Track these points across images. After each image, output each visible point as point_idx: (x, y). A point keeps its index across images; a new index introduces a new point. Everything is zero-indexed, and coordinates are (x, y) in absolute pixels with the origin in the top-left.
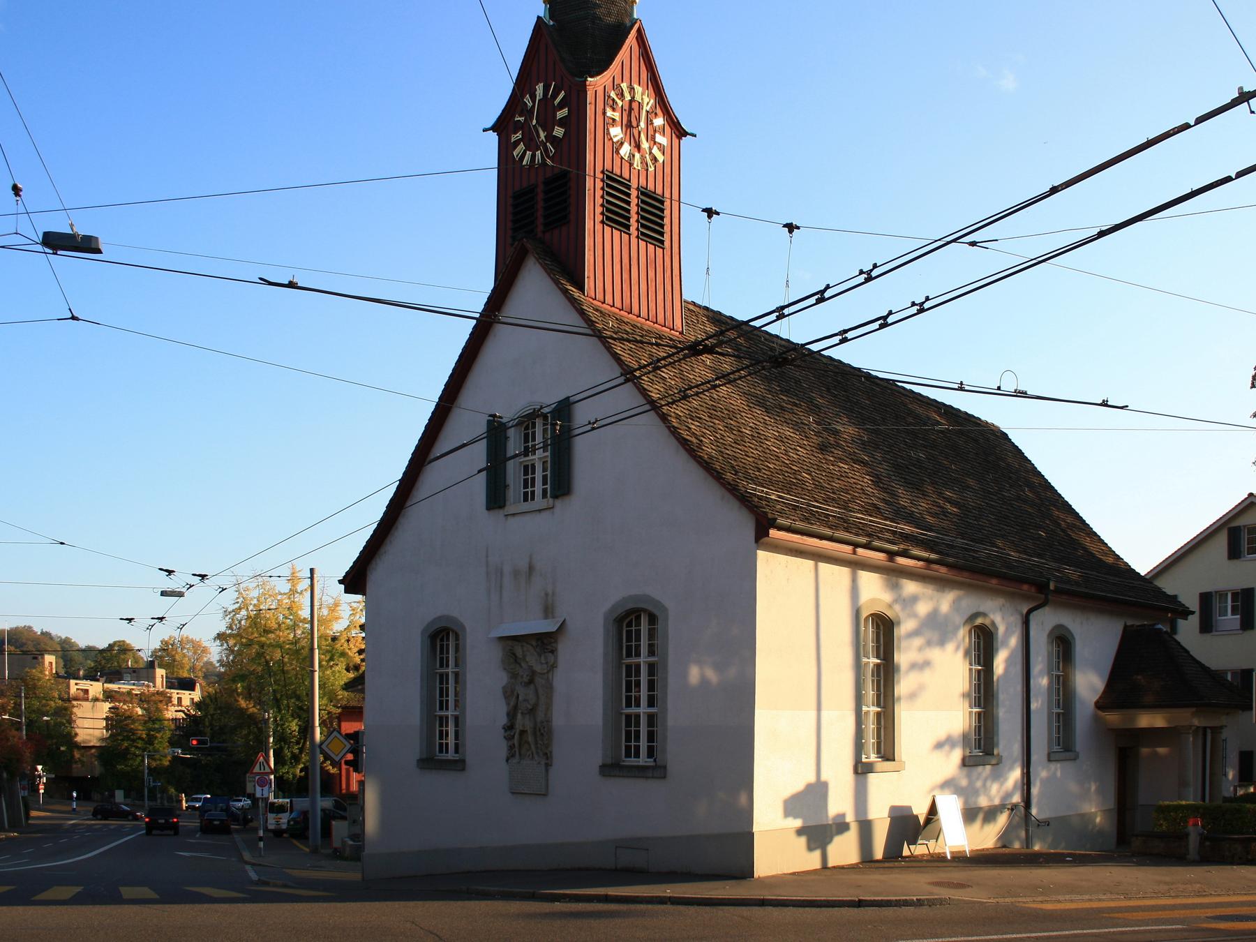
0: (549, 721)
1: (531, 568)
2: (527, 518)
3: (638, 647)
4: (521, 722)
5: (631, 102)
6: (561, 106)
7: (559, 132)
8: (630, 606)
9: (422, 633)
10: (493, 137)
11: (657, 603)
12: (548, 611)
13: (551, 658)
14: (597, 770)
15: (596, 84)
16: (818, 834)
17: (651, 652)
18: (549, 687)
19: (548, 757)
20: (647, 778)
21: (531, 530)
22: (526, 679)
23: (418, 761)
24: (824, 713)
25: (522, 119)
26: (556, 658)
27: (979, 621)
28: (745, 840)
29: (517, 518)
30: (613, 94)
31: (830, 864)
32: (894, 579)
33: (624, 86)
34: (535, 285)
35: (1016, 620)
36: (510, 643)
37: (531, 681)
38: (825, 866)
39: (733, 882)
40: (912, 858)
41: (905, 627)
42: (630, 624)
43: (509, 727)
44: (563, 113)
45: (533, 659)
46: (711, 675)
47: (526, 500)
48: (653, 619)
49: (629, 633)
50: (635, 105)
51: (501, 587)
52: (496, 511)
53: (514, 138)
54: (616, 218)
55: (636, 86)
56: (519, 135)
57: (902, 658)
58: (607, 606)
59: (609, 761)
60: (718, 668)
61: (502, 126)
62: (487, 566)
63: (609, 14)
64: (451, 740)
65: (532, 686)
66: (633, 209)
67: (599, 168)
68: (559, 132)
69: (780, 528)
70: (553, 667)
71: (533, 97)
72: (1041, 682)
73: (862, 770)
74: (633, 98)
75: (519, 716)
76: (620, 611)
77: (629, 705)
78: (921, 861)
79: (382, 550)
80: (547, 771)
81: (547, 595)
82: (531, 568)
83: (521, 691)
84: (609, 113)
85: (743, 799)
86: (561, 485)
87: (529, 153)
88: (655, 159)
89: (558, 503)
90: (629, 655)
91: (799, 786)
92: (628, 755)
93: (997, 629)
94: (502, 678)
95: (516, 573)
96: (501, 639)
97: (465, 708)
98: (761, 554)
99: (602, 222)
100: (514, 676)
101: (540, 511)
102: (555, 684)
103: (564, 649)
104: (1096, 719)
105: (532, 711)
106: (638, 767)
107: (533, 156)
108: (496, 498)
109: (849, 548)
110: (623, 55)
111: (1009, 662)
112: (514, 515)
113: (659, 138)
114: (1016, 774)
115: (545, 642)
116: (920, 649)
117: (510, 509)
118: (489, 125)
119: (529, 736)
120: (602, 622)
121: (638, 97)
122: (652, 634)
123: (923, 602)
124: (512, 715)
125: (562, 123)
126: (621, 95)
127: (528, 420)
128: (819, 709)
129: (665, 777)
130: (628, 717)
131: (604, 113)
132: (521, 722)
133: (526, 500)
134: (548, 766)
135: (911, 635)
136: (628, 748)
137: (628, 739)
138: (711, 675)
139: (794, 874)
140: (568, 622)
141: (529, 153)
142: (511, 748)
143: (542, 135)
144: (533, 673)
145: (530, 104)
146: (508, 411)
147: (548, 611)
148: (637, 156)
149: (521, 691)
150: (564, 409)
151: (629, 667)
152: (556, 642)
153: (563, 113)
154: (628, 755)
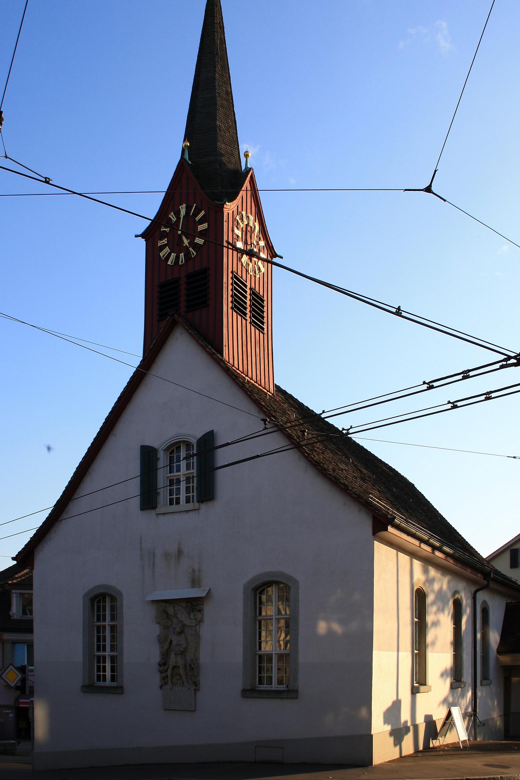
0: (197, 659)
1: (180, 552)
2: (176, 517)
3: (104, 616)
5: (247, 225)
6: (201, 222)
7: (199, 241)
8: (102, 591)
9: (84, 596)
10: (142, 242)
11: (290, 578)
13: (199, 616)
15: (230, 207)
16: (398, 734)
17: (113, 618)
18: (197, 637)
19: (196, 684)
20: (281, 698)
21: (176, 524)
22: (178, 630)
23: (242, 691)
24: (400, 653)
25: (167, 230)
26: (203, 615)
27: (457, 596)
28: (367, 740)
29: (166, 517)
30: (238, 218)
31: (403, 755)
32: (427, 565)
33: (244, 213)
34: (181, 348)
35: (470, 595)
36: (163, 604)
37: (181, 632)
38: (401, 756)
39: (361, 769)
40: (434, 748)
41: (430, 598)
42: (99, 602)
43: (163, 664)
45: (183, 616)
46: (337, 628)
47: (171, 503)
48: (113, 599)
49: (99, 607)
50: (249, 229)
51: (154, 565)
52: (149, 512)
53: (205, 226)
54: (238, 307)
55: (250, 215)
56: (165, 241)
57: (430, 618)
59: (249, 687)
60: (341, 622)
61: (148, 235)
62: (141, 550)
63: (230, 162)
64: (108, 673)
65: (183, 635)
67: (230, 270)
69: (398, 527)
70: (201, 621)
71: (177, 213)
72: (479, 636)
73: (414, 691)
74: (249, 223)
75: (173, 656)
77: (99, 650)
78: (443, 750)
80: (195, 694)
81: (194, 571)
82: (180, 552)
83: (175, 639)
84: (236, 231)
85: (364, 712)
86: (206, 491)
87: (173, 255)
88: (259, 269)
89: (203, 506)
90: (98, 620)
91: (389, 704)
92: (99, 680)
93: (463, 601)
94: (155, 630)
95: (167, 555)
96: (154, 602)
98: (377, 545)
99: (232, 308)
100: (166, 628)
101: (187, 511)
103: (208, 609)
104: (497, 659)
105: (183, 653)
106: (107, 687)
107: (177, 257)
108: (148, 500)
109: (417, 543)
110: (242, 193)
111: (467, 621)
112: (164, 514)
114: (469, 694)
115: (194, 605)
116: (436, 613)
118: (140, 233)
119: (179, 669)
120: (241, 590)
121: (251, 224)
122: (113, 608)
123: (441, 583)
124: (165, 655)
125: (202, 234)
126: (242, 219)
127: (174, 448)
128: (398, 651)
129: (297, 698)
130: (99, 657)
131: (233, 231)
132: (173, 660)
133: (171, 503)
135: (433, 603)
136: (99, 676)
137: (99, 671)
138: (337, 628)
139: (389, 762)
141: (173, 255)
142: (164, 678)
143: (186, 242)
145: (174, 219)
147: (195, 582)
148: (251, 265)
150: (208, 445)
151: (98, 628)
152: (203, 604)
154: (99, 680)
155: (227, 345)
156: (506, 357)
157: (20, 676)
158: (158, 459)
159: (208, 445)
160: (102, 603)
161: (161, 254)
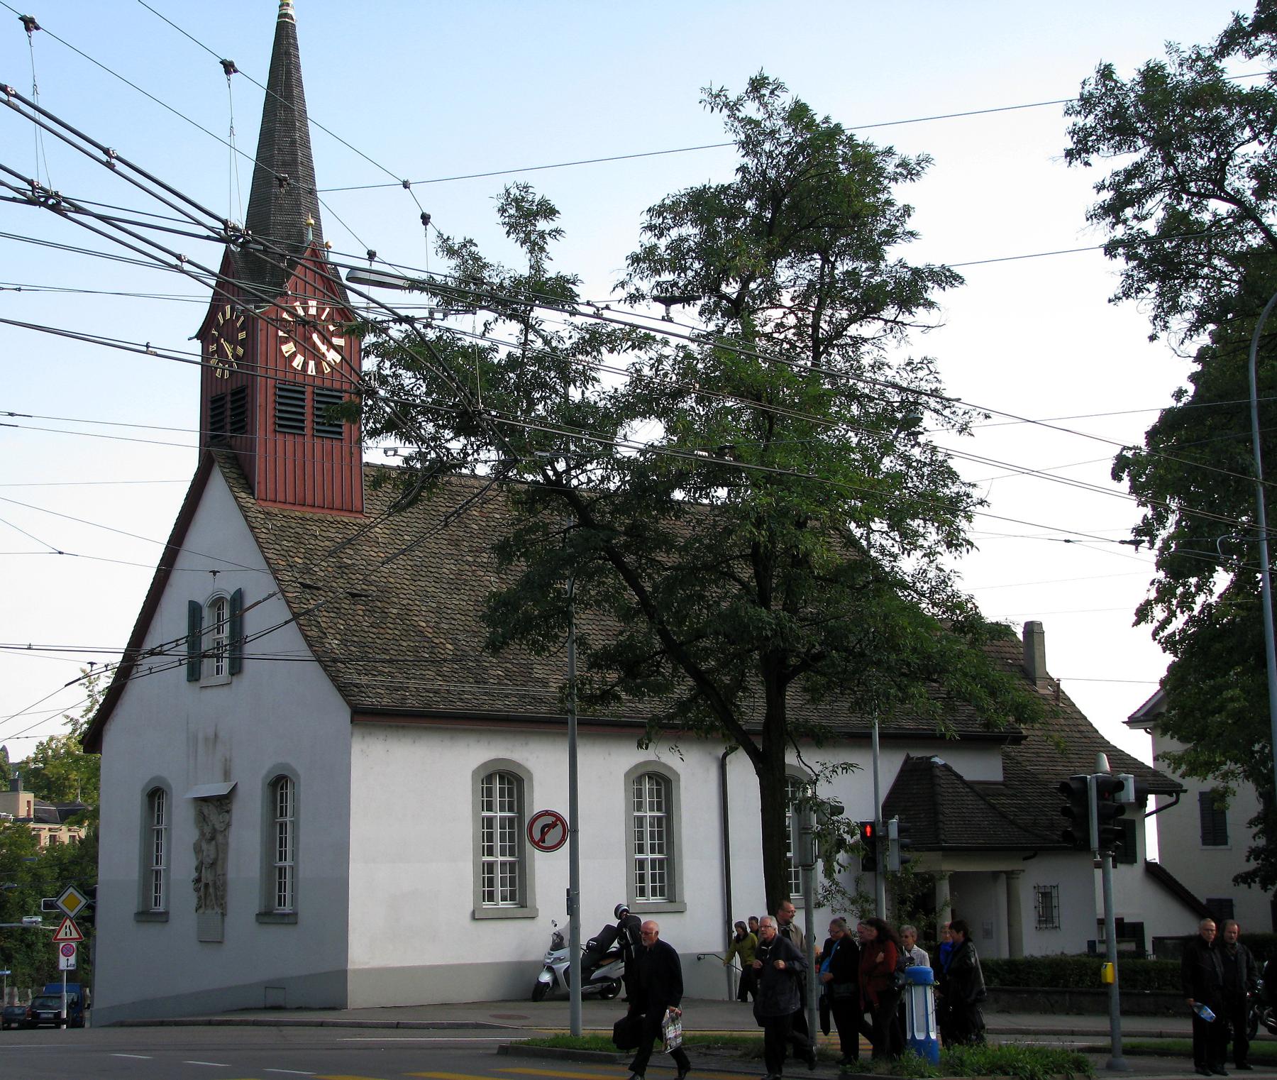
1: (216, 736)
4: (207, 876)
12: (227, 775)
14: (254, 917)
19: (223, 906)
31: (217, 270)
37: (213, 838)
44: (242, 335)
45: (215, 818)
54: (289, 423)
58: (264, 772)
61: (202, 335)
66: (308, 411)
68: (240, 351)
70: (228, 825)
76: (272, 776)
79: (115, 712)
80: (223, 921)
82: (216, 736)
89: (235, 678)
96: (196, 799)
97: (474, 820)
100: (202, 834)
102: (230, 840)
103: (237, 807)
113: (336, 341)
115: (222, 802)
117: (203, 682)
124: (198, 869)
127: (217, 603)
129: (1230, 901)
134: (223, 915)
140: (239, 786)
142: (199, 898)
144: (214, 831)
146: (202, 598)
147: (227, 775)
149: (204, 846)
150: (238, 597)
151: (281, 825)
153: (242, 335)
155: (263, 482)
156: (566, 817)
157: (84, 902)
158: (202, 618)
159: (238, 597)
160: (156, 796)
161: (295, 364)
